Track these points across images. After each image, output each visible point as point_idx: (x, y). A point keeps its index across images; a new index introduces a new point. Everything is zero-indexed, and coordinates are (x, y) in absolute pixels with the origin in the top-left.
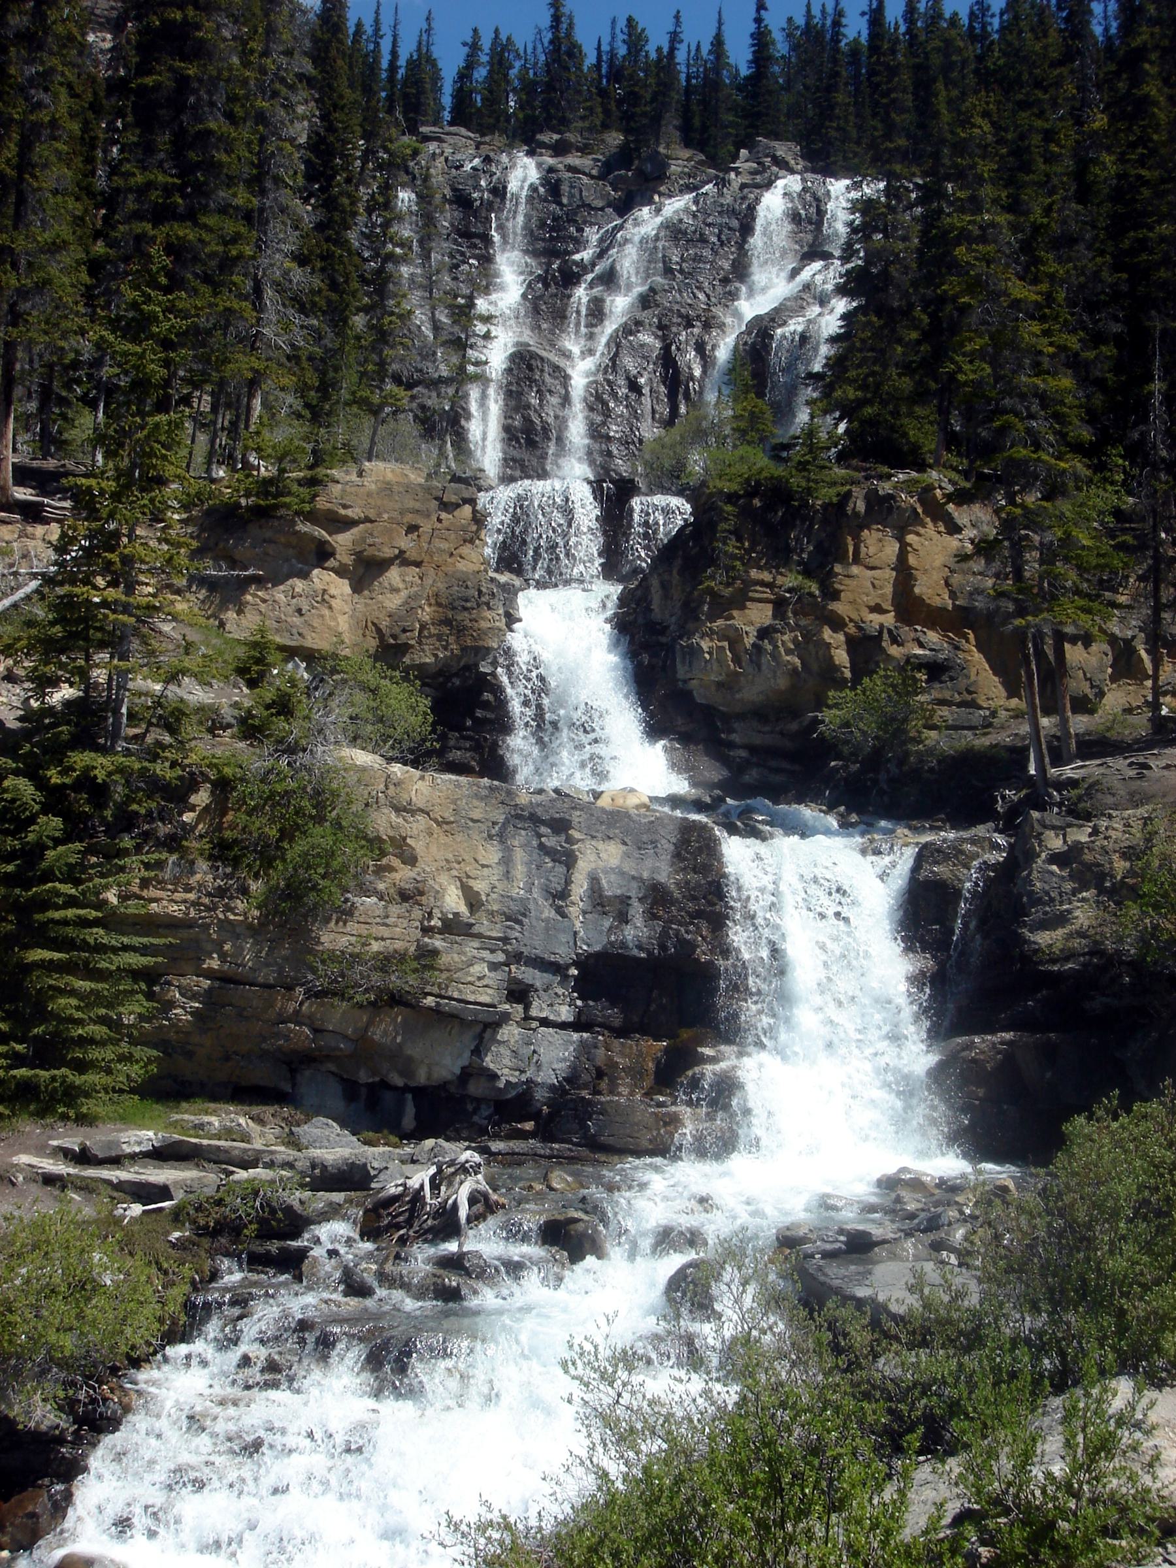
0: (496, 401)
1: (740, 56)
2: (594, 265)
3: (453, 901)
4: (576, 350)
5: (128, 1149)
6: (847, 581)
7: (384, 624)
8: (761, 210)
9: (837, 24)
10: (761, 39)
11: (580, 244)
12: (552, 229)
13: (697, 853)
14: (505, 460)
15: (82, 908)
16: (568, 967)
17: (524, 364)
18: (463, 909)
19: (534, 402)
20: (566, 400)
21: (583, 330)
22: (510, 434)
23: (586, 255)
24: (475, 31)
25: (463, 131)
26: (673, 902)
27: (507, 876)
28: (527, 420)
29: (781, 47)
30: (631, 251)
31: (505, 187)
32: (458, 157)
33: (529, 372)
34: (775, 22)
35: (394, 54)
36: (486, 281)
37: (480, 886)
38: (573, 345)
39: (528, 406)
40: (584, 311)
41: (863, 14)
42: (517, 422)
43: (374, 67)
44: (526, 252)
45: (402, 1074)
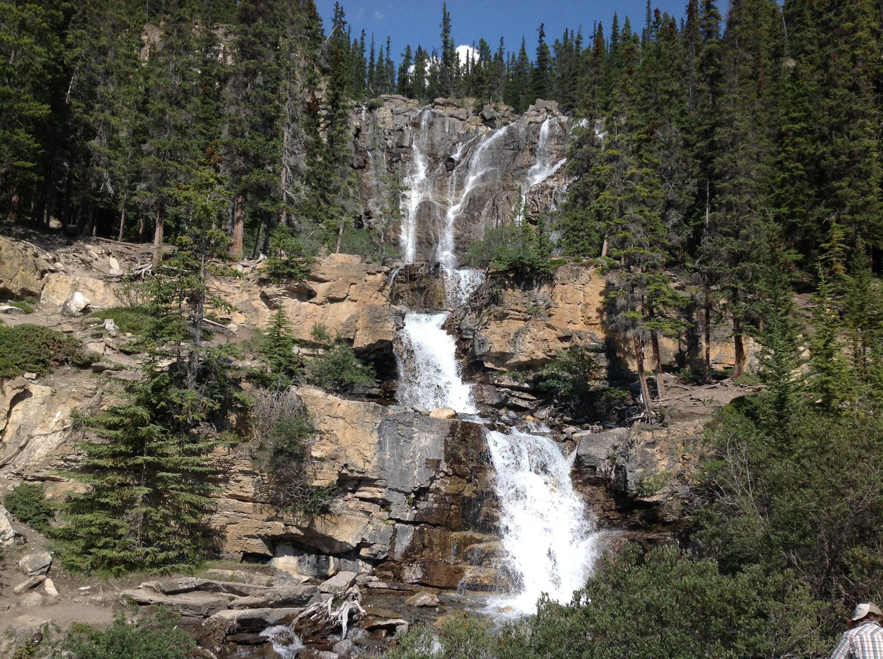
1: (532, 57)
4: (451, 202)
5: (181, 587)
6: (556, 310)
8: (542, 128)
9: (578, 43)
10: (542, 51)
15: (176, 473)
16: (410, 494)
17: (425, 207)
29: (552, 54)
33: (427, 214)
34: (549, 41)
35: (372, 59)
41: (591, 37)
43: (361, 64)
45: (328, 546)
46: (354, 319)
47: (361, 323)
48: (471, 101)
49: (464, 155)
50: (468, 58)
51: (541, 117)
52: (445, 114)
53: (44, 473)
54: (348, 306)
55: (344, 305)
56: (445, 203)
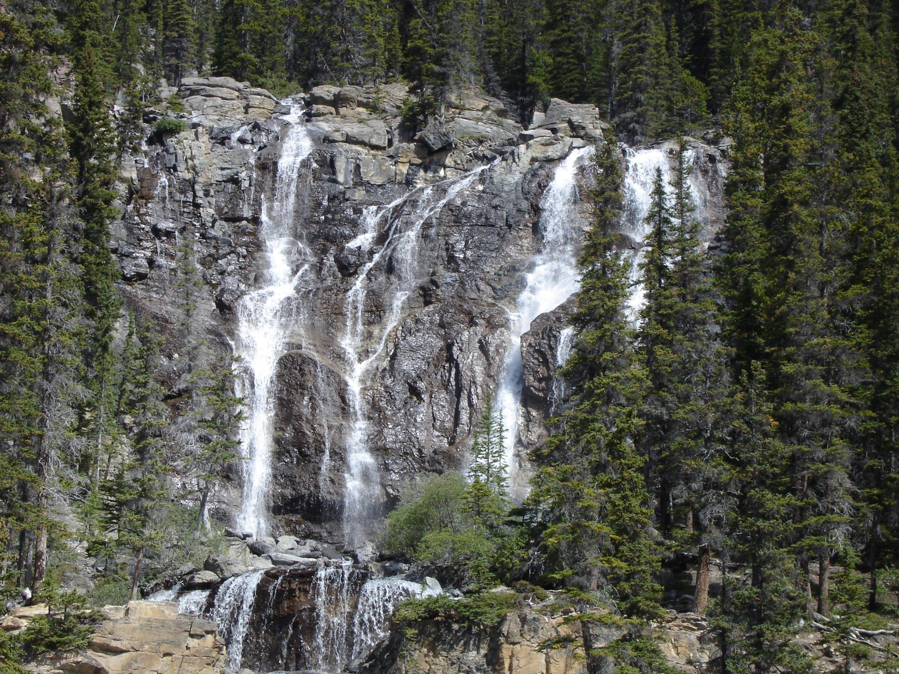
0: (267, 411)
2: (371, 253)
11: (356, 226)
12: (327, 211)
14: (275, 476)
17: (293, 370)
20: (344, 408)
21: (360, 327)
22: (280, 450)
23: (364, 240)
25: (231, 82)
28: (298, 432)
30: (412, 234)
31: (275, 164)
32: (225, 124)
36: (254, 276)
38: (348, 343)
39: (299, 417)
40: (360, 307)
42: (289, 434)
48: (398, 92)
49: (382, 239)
51: (559, 146)
52: (337, 136)
56: (340, 356)
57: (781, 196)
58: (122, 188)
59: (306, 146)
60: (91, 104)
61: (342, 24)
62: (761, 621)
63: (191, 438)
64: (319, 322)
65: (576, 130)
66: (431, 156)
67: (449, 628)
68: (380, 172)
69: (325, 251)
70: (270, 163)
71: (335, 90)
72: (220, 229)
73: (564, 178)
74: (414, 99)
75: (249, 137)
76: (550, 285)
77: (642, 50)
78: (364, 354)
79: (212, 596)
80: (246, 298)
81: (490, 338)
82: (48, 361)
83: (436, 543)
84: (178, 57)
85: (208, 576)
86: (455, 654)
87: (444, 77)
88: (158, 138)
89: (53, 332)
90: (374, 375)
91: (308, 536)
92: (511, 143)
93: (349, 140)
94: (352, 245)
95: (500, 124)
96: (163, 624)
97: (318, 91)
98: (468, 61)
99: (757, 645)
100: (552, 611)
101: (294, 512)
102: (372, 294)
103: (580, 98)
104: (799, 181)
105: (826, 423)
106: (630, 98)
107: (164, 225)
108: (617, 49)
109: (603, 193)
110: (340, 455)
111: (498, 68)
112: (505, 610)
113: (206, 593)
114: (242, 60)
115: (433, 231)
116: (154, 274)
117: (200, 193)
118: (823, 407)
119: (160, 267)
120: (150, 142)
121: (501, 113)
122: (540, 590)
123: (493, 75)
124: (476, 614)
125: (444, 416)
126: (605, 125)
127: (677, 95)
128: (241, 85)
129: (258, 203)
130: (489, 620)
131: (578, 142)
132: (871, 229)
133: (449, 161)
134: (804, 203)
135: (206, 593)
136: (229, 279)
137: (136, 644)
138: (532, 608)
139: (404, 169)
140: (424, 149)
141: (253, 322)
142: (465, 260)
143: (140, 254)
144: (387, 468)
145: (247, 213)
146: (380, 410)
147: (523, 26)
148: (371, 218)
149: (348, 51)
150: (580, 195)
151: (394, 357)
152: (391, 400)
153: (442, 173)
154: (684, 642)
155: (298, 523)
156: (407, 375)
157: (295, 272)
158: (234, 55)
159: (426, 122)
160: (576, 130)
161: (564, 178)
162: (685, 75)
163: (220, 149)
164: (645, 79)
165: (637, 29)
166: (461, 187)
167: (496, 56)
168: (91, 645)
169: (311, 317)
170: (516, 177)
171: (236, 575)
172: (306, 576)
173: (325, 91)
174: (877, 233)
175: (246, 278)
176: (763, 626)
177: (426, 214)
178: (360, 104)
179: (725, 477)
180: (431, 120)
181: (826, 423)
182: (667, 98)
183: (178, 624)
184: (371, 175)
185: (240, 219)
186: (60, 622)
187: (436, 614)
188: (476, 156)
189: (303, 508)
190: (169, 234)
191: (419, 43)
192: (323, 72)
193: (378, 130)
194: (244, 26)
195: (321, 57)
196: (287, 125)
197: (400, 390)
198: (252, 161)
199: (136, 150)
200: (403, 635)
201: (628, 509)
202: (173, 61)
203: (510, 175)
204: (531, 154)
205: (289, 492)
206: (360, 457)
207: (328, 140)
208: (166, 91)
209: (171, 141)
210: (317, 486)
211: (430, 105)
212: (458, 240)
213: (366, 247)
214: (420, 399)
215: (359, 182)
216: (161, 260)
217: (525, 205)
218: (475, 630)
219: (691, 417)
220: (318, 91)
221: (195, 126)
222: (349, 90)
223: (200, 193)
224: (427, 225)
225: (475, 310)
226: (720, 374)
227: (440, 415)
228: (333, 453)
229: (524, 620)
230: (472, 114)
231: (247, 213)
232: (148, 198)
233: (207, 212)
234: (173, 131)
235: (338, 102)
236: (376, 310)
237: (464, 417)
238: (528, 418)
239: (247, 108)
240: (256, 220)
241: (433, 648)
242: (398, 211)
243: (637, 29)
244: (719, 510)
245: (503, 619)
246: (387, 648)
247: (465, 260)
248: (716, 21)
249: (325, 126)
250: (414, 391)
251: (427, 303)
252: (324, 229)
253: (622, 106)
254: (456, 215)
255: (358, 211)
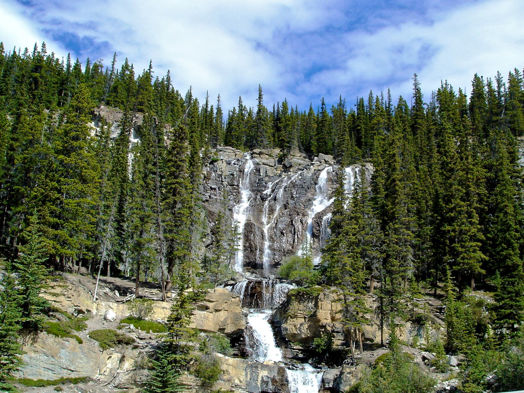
2: (270, 195)
3: (237, 381)
7: (220, 324)
8: (321, 176)
11: (266, 187)
13: (281, 372)
17: (249, 226)
18: (239, 383)
19: (252, 238)
22: (245, 249)
23: (268, 191)
24: (234, 108)
26: (277, 382)
27: (247, 377)
28: (250, 244)
30: (281, 190)
37: (241, 379)
38: (264, 220)
39: (250, 240)
44: (250, 190)
46: (226, 319)
47: (229, 322)
48: (277, 151)
49: (273, 191)
50: (274, 109)
51: (322, 166)
52: (260, 163)
53: (127, 386)
54: (224, 313)
55: (222, 313)
56: (262, 223)
57: (393, 179)
58: (202, 176)
59: (252, 166)
60: (195, 153)
61: (261, 133)
62: (392, 295)
63: (226, 244)
64: (256, 213)
65: (326, 162)
66: (286, 169)
67: (304, 297)
68: (272, 173)
69: (257, 194)
70: (242, 170)
71: (259, 150)
72: (229, 188)
73: (323, 175)
74: (281, 153)
75: (236, 163)
76: (320, 204)
77: (344, 141)
78: (268, 223)
79: (233, 288)
80: (236, 207)
81: (303, 219)
82: (192, 221)
83: (295, 275)
84: (216, 141)
85: (232, 282)
86: (305, 304)
87: (290, 147)
88: (212, 163)
89: (194, 212)
90: (271, 228)
91: (253, 273)
92: (308, 165)
93: (264, 164)
94: (265, 192)
95: (305, 160)
96: (225, 294)
97: (254, 151)
98: (296, 142)
99: (392, 302)
100: (333, 292)
101: (249, 266)
102: (270, 206)
103: (326, 153)
104: (398, 175)
105: (406, 241)
106: (340, 154)
107: (213, 187)
108: (337, 141)
109: (338, 179)
110: (262, 251)
111: (303, 145)
112: (319, 292)
113: (231, 287)
114: (232, 143)
115: (287, 189)
116: (211, 200)
117: (223, 178)
118: (406, 237)
119: (212, 198)
120: (210, 164)
121: (305, 157)
122: (329, 287)
123: (302, 147)
124: (311, 293)
125: (290, 240)
126: (334, 161)
127: (354, 153)
128: (233, 149)
129: (239, 180)
130: (315, 295)
131: (327, 165)
132: (414, 189)
133: (291, 170)
134: (400, 181)
135: (231, 287)
136: (231, 202)
137: (217, 300)
138: (327, 292)
139: (279, 172)
140: (284, 166)
141: (238, 213)
142: (296, 197)
143: (207, 194)
144: (275, 255)
145: (236, 184)
146: (273, 238)
147: (310, 134)
148: (270, 185)
149: (262, 140)
150: (329, 180)
151: (276, 224)
152: (276, 235)
153: (289, 173)
154: (369, 301)
155: (250, 269)
156: (280, 229)
157: (249, 200)
158: (230, 141)
159: (285, 159)
160: (326, 162)
161: (323, 175)
162: (356, 148)
163: (229, 166)
164: (344, 149)
165: (342, 135)
166: (295, 177)
167: (302, 142)
168: (205, 300)
169: (254, 213)
170: (310, 175)
171: (240, 282)
172: (260, 283)
173: (257, 151)
174: (416, 190)
175: (236, 201)
176: (393, 297)
177: (285, 184)
178: (266, 154)
179: (379, 256)
180: (286, 159)
181: (406, 241)
182: (351, 154)
183: (229, 294)
184: (270, 174)
185: (234, 185)
186: (196, 293)
187: (300, 293)
188: (299, 169)
189: (252, 265)
190: (215, 189)
191: (283, 138)
192: (255, 145)
193: (272, 161)
194: (233, 133)
195: (255, 142)
196: (247, 160)
197: (278, 233)
198: (237, 169)
199: (206, 166)
200: (291, 298)
201: (356, 264)
202: (215, 142)
203: (309, 174)
204: (314, 168)
205: (247, 260)
206: (267, 251)
207: (258, 164)
208: (214, 151)
209: (215, 164)
210: (255, 259)
211: (286, 155)
212: (294, 192)
213: (268, 194)
214: (284, 235)
215: (267, 176)
216: (212, 196)
217: (313, 182)
218: (311, 297)
219: (369, 239)
220: (254, 151)
221: (222, 160)
222: (263, 151)
223: (223, 178)
224: (285, 187)
225: (299, 211)
226: (377, 228)
227: (290, 240)
228: (260, 250)
229: (325, 295)
230: (297, 157)
231: (236, 184)
232: (209, 179)
233: (225, 183)
234: (216, 161)
235: (260, 154)
236: (272, 211)
237: (296, 241)
238: (314, 241)
239: (236, 155)
240: (238, 186)
241: (299, 302)
242: (277, 184)
243: (342, 135)
244: (377, 265)
245: (319, 294)
246: (286, 302)
247: (296, 197)
248: (363, 133)
249: (257, 160)
250: (282, 233)
251: (286, 209)
252: (257, 188)
253: (338, 156)
254: (294, 185)
255: (266, 183)
